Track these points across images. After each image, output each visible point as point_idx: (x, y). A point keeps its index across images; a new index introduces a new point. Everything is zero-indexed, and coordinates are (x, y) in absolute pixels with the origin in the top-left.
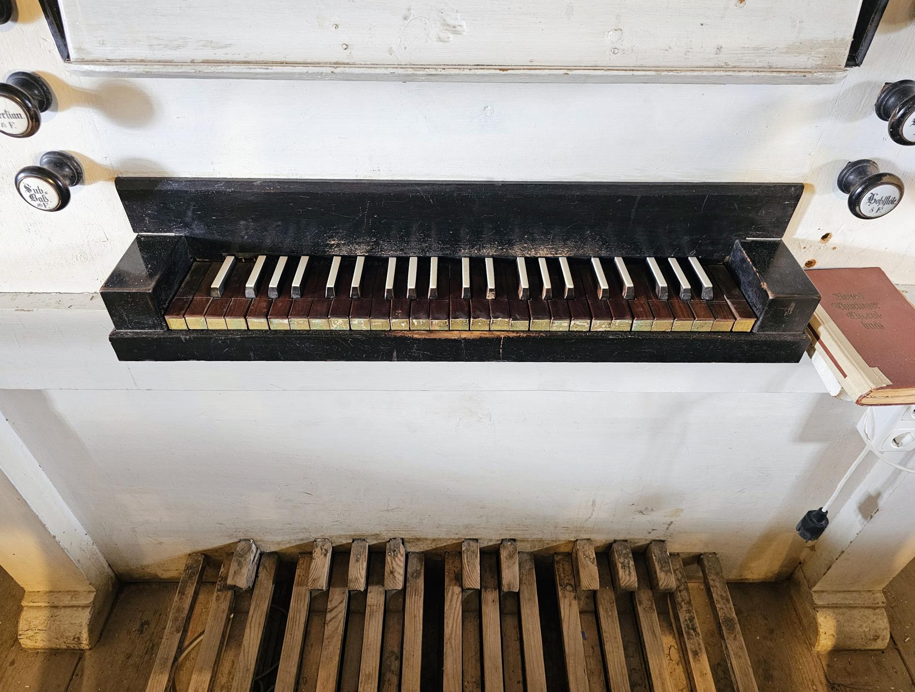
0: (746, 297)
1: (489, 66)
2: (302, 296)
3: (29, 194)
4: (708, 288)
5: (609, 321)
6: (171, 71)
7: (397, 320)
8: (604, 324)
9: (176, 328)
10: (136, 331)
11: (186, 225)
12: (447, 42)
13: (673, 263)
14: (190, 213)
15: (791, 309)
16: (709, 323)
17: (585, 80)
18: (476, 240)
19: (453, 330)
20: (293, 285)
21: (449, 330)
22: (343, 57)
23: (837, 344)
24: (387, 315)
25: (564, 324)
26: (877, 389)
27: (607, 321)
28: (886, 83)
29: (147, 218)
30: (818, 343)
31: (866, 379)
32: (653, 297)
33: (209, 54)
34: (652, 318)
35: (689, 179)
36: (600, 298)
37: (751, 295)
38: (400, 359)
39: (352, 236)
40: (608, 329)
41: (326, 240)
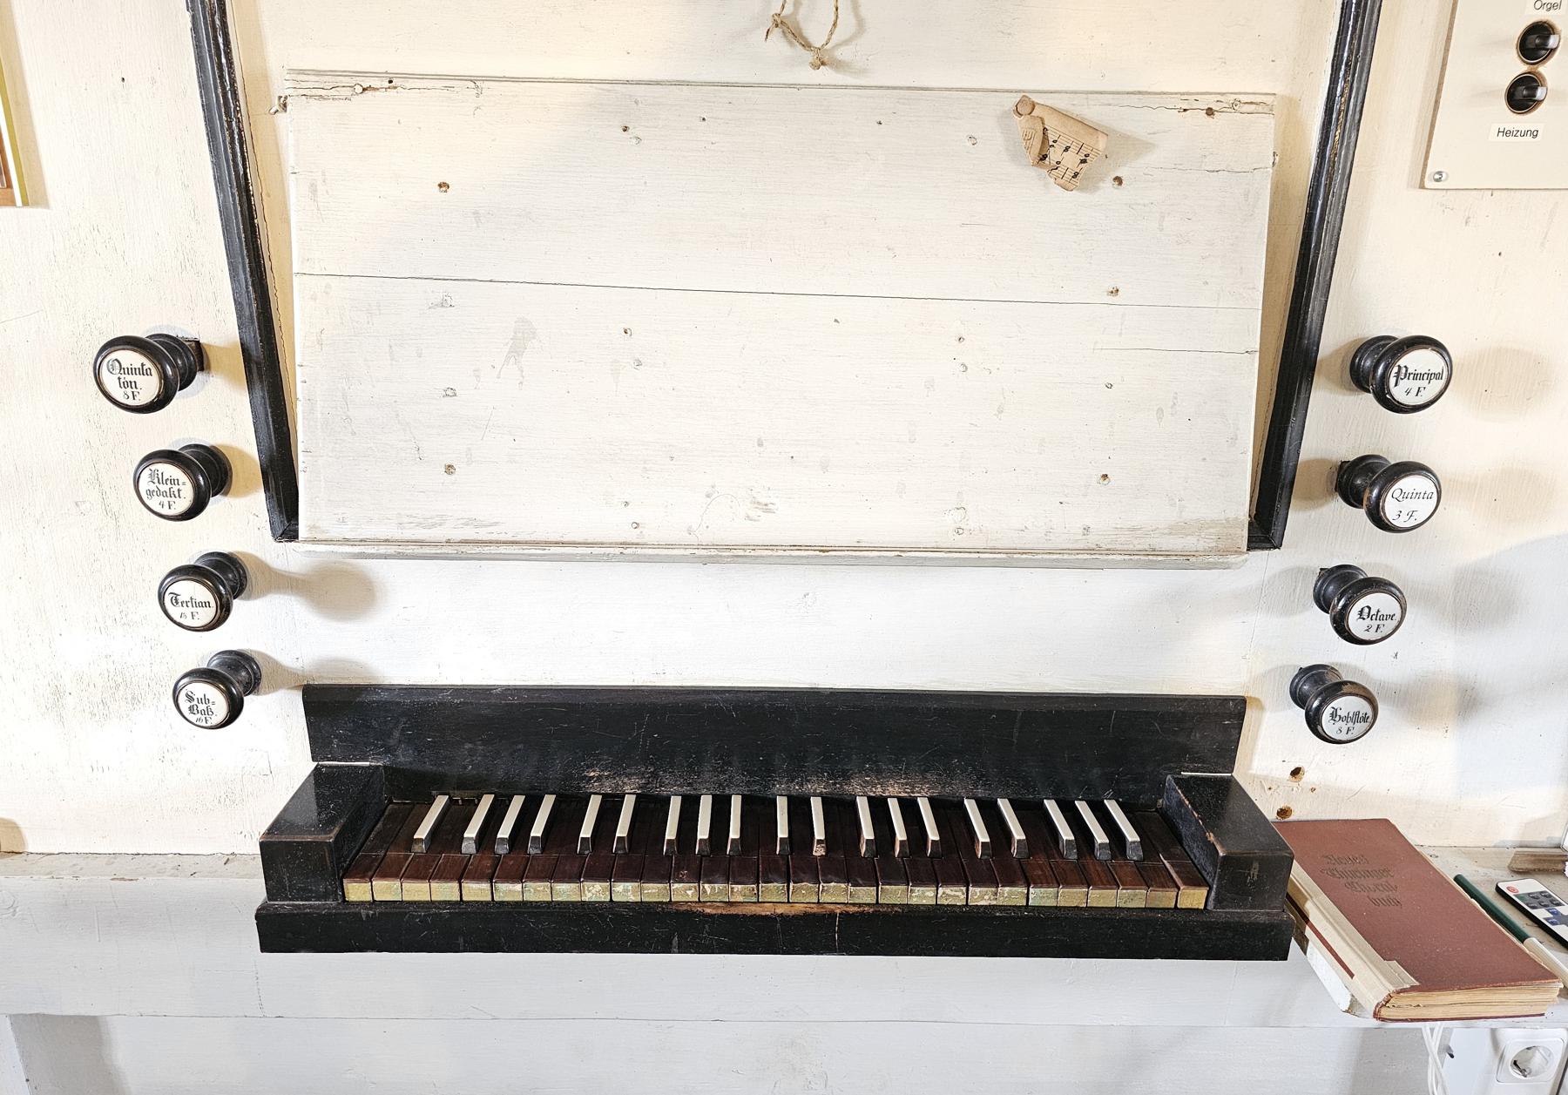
0: (1192, 857)
1: (808, 547)
2: (543, 850)
3: (189, 704)
4: (1134, 842)
5: (994, 889)
6: (428, 551)
7: (682, 885)
8: (986, 893)
9: (355, 899)
10: (297, 903)
11: (389, 750)
12: (758, 521)
13: (1082, 807)
14: (397, 734)
15: (1255, 871)
16: (1141, 894)
17: (922, 563)
18: (797, 770)
19: (764, 902)
20: (533, 834)
21: (758, 902)
22: (632, 536)
23: (1334, 927)
24: (666, 877)
25: (927, 894)
26: (1398, 993)
27: (990, 889)
28: (1321, 569)
29: (335, 741)
30: (1307, 928)
31: (1381, 977)
32: (1056, 856)
33: (470, 533)
34: (1056, 885)
35: (1087, 689)
36: (979, 856)
37: (1197, 853)
38: (683, 950)
39: (619, 766)
40: (994, 903)
41: (584, 771)
